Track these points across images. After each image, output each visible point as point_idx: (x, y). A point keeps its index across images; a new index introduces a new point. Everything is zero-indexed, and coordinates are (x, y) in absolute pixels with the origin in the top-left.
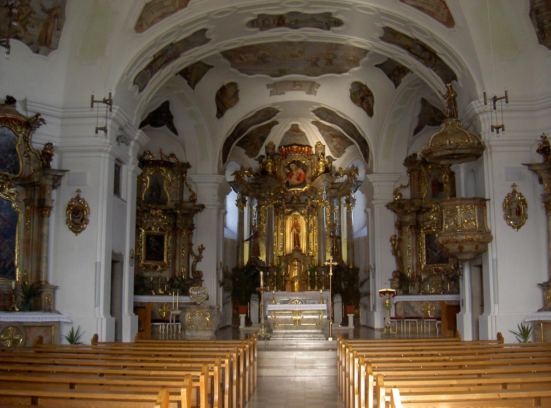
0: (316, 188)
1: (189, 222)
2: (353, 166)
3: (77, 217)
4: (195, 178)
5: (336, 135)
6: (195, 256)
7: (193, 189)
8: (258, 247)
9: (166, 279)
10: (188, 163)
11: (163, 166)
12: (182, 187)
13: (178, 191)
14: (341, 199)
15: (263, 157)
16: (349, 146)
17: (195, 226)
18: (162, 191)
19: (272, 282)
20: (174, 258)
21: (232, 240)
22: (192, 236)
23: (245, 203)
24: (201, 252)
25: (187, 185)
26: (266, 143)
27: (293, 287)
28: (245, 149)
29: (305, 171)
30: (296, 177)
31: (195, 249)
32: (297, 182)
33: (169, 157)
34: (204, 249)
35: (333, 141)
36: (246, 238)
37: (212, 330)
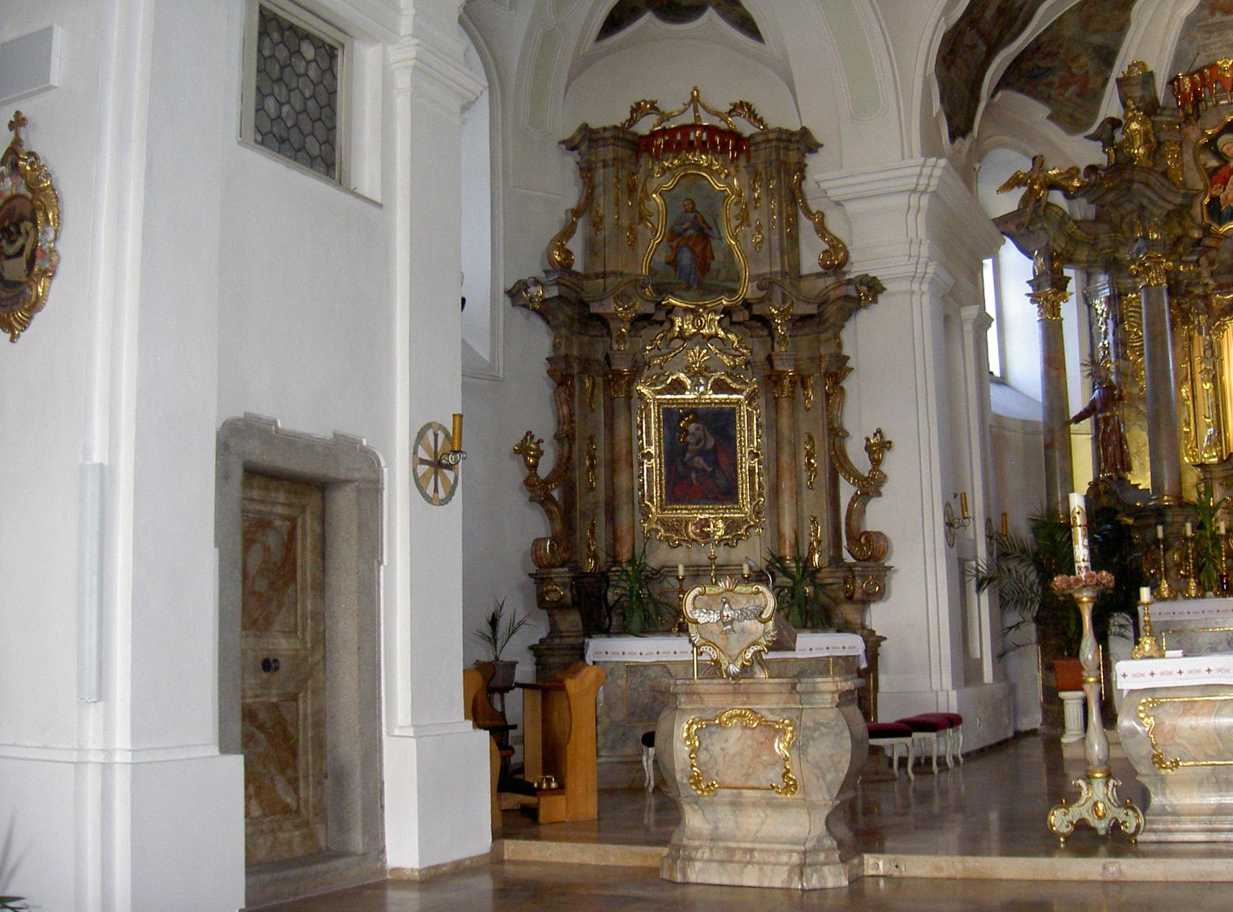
1: (826, 350)
3: (11, 250)
7: (834, 225)
8: (1121, 440)
10: (805, 132)
11: (702, 147)
12: (793, 226)
13: (775, 238)
15: (1114, 123)
17: (850, 364)
18: (714, 243)
19: (1179, 566)
21: (1025, 423)
22: (842, 403)
23: (1064, 288)
24: (876, 463)
25: (808, 213)
26: (1119, 69)
28: (1046, 100)
33: (730, 113)
34: (885, 445)
37: (810, 807)
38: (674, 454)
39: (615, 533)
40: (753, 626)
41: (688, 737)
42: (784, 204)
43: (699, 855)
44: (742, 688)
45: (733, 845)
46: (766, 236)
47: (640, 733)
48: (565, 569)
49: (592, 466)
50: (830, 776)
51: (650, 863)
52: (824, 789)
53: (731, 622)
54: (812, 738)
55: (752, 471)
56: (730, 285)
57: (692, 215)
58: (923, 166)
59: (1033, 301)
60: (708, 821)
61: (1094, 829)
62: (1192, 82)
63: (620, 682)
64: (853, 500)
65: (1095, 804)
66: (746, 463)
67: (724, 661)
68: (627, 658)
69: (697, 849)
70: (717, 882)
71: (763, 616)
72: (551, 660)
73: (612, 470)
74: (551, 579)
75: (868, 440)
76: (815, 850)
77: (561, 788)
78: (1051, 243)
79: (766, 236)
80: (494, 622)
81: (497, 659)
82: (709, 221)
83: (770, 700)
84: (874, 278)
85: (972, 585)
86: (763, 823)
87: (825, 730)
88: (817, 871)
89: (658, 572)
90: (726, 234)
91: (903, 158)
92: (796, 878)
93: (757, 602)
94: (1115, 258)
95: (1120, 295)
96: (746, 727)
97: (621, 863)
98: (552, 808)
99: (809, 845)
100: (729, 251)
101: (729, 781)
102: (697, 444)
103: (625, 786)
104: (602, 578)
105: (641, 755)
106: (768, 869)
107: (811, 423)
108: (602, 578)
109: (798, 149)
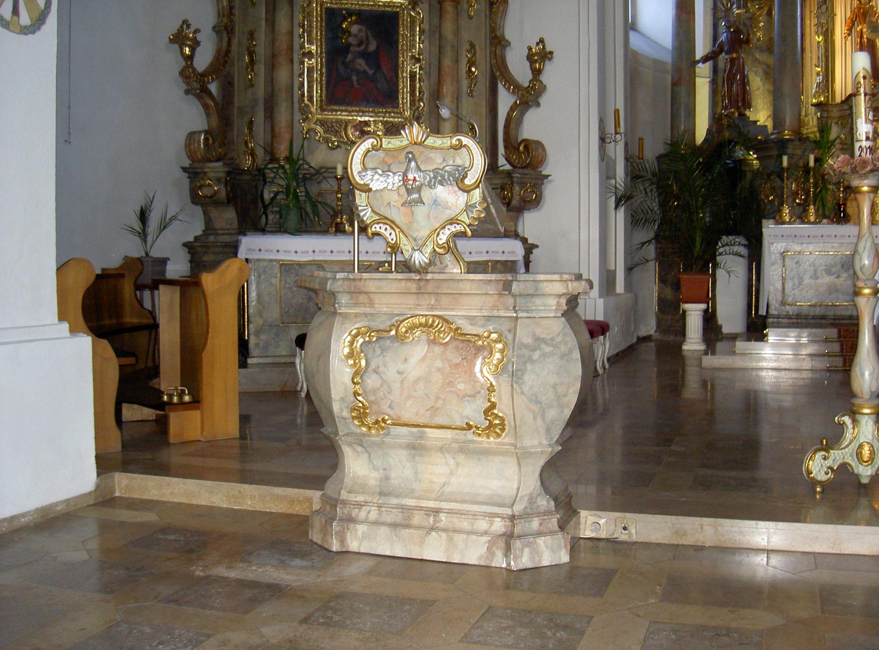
21: (656, 62)
22: (505, 11)
31: (517, 65)
36: (700, 53)
37: (521, 456)
38: (336, 53)
39: (273, 130)
40: (452, 199)
41: (351, 355)
43: (362, 515)
44: (430, 288)
45: (411, 502)
47: (294, 334)
48: (220, 164)
49: (252, 61)
50: (552, 414)
51: (297, 509)
52: (542, 431)
53: (419, 190)
54: (530, 360)
55: (413, 76)
60: (375, 468)
61: (857, 477)
63: (273, 281)
64: (512, 109)
65: (861, 446)
66: (408, 67)
67: (406, 246)
68: (281, 257)
69: (360, 505)
70: (388, 554)
71: (467, 182)
72: (205, 258)
73: (272, 66)
74: (205, 173)
75: (530, 49)
76: (526, 515)
77: (196, 402)
80: (143, 216)
81: (147, 255)
83: (473, 302)
85: (612, 202)
86: (452, 474)
87: (548, 349)
88: (529, 545)
89: (318, 172)
92: (499, 554)
93: (459, 162)
96: (433, 342)
97: (259, 507)
98: (185, 425)
99: (518, 508)
101: (407, 417)
102: (359, 45)
103: (278, 389)
104: (260, 174)
105: (294, 356)
106: (459, 538)
107: (473, 31)
108: (260, 174)
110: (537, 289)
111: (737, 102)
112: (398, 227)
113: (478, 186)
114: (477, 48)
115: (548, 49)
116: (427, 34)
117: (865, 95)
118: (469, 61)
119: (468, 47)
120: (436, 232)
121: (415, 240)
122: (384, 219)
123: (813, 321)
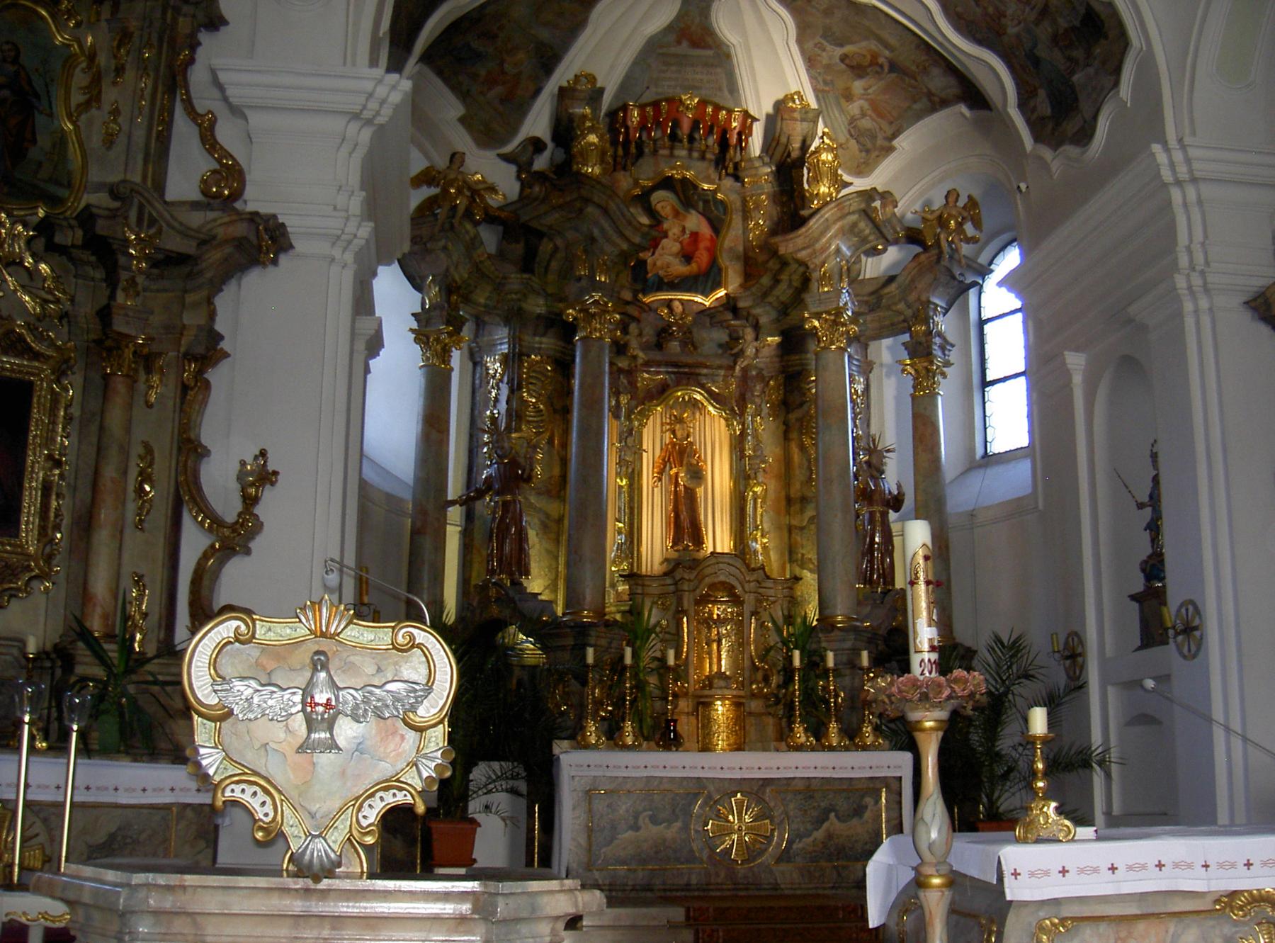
0: (803, 263)
1: (192, 319)
2: (951, 195)
4: (240, 84)
5: (874, 62)
6: (217, 522)
7: (226, 134)
9: (23, 643)
14: (873, 345)
15: (536, 145)
16: (919, 117)
17: (224, 345)
18: (40, 120)
20: (85, 524)
21: (389, 497)
22: (204, 403)
24: (250, 502)
26: (562, 76)
27: (706, 724)
28: (464, 95)
29: (717, 226)
30: (676, 247)
31: (219, 482)
32: (679, 268)
35: (848, 97)
42: (160, 89)
46: (125, 128)
55: (47, 488)
56: (53, 189)
57: (12, 68)
58: (380, 81)
59: (417, 340)
62: (643, 116)
64: (205, 557)
75: (243, 463)
78: (452, 269)
79: (125, 128)
82: (38, 83)
84: (283, 224)
90: (60, 110)
91: (345, 64)
94: (520, 309)
95: (521, 354)
100: (61, 141)
109: (194, 16)
110: (534, 910)
111: (510, 564)
112: (280, 792)
113: (441, 722)
114: (156, 455)
115: (270, 468)
116: (76, 423)
117: (928, 583)
118: (141, 474)
119: (141, 450)
120: (359, 802)
121: (313, 816)
122: (251, 775)
123: (633, 894)
